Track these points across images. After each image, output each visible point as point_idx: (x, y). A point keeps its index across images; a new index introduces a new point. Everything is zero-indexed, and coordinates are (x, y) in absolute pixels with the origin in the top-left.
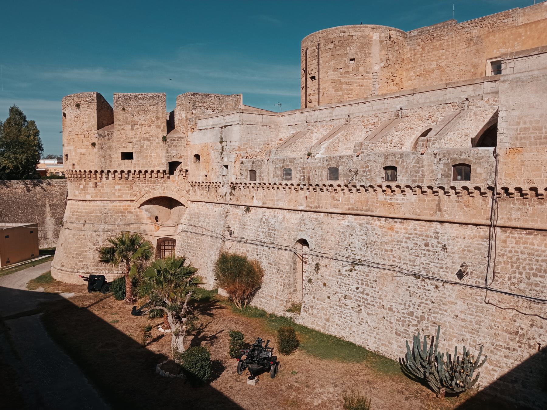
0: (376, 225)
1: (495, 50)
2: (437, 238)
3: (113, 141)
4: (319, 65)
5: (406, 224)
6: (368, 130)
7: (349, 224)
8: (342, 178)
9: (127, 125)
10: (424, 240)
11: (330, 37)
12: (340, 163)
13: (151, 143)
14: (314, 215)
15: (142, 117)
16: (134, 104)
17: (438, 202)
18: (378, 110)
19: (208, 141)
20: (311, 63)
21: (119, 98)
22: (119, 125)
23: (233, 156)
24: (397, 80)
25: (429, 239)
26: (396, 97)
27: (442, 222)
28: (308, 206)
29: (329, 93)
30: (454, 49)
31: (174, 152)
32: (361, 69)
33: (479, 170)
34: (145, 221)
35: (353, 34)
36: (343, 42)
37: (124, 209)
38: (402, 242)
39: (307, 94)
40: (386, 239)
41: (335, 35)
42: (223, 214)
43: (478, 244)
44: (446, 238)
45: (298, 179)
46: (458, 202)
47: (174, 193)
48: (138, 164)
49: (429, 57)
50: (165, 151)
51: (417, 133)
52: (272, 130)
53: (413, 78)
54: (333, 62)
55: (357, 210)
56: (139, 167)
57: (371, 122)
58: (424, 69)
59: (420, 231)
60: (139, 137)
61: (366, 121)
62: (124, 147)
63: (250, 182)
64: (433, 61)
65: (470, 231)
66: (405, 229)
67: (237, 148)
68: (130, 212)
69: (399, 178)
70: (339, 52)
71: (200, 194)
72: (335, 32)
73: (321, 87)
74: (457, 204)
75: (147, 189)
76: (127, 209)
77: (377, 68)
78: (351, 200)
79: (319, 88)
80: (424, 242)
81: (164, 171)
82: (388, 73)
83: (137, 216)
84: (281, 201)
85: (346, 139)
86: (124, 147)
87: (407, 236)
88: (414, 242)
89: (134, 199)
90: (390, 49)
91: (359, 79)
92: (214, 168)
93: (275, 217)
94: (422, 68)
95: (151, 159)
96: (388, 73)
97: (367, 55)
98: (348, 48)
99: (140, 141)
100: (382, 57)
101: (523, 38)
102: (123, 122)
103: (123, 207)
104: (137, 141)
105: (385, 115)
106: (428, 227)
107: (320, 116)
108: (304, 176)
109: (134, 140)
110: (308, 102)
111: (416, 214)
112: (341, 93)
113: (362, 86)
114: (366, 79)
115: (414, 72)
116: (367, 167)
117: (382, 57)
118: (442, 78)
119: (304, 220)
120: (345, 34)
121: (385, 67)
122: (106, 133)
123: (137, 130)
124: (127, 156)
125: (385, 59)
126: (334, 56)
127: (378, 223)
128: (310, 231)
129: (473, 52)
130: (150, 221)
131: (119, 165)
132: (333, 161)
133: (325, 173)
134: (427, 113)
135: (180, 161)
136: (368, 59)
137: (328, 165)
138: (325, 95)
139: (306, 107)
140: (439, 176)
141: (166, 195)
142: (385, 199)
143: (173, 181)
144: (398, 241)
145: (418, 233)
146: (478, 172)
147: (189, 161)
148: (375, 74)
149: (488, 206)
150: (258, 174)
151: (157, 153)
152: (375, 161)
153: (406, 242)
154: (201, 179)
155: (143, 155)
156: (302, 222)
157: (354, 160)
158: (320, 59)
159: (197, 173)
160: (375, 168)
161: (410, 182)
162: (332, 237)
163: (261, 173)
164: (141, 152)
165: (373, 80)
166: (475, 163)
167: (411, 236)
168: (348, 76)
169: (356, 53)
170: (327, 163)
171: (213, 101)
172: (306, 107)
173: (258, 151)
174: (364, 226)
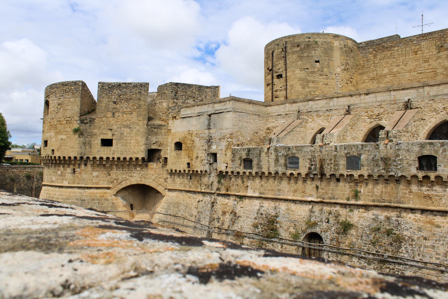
4: (286, 65)
6: (372, 120)
11: (296, 41)
12: (362, 152)
13: (132, 131)
15: (125, 105)
16: (117, 93)
18: (384, 101)
19: (192, 129)
20: (278, 63)
21: (103, 87)
23: (224, 144)
24: (354, 82)
28: (320, 197)
31: (154, 139)
32: (325, 70)
34: (120, 209)
35: (317, 40)
36: (308, 46)
37: (100, 196)
39: (274, 90)
41: (301, 40)
47: (151, 181)
48: (117, 151)
50: (144, 139)
51: (430, 124)
52: (260, 119)
53: (366, 81)
54: (300, 63)
55: (384, 202)
56: (118, 153)
57: (376, 113)
58: (376, 74)
62: (104, 134)
63: (244, 170)
64: (385, 67)
67: (229, 136)
68: (106, 199)
69: (439, 168)
70: (305, 55)
71: (179, 183)
72: (301, 38)
73: (288, 84)
75: (124, 176)
76: (103, 196)
77: (338, 70)
79: (286, 85)
81: (143, 159)
82: (346, 75)
83: (113, 203)
85: (352, 128)
86: (104, 134)
89: (110, 186)
91: (323, 78)
92: (199, 156)
94: (375, 73)
96: (346, 75)
98: (313, 52)
99: (121, 128)
100: (342, 61)
103: (100, 193)
104: (118, 128)
105: (392, 106)
107: (314, 106)
109: (115, 127)
110: (274, 97)
112: (308, 90)
114: (330, 79)
115: (368, 76)
117: (342, 61)
120: (310, 40)
121: (345, 70)
122: (88, 120)
124: (107, 143)
125: (344, 63)
126: (301, 58)
130: (125, 209)
131: (98, 151)
132: (353, 149)
135: (160, 148)
138: (292, 91)
139: (272, 101)
141: (143, 183)
143: (151, 168)
147: (169, 148)
148: (337, 75)
150: (255, 163)
152: (408, 150)
154: (182, 167)
158: (287, 60)
159: (178, 162)
160: (408, 158)
168: (314, 75)
169: (321, 56)
170: (346, 152)
171: (194, 91)
172: (272, 101)
173: (248, 139)
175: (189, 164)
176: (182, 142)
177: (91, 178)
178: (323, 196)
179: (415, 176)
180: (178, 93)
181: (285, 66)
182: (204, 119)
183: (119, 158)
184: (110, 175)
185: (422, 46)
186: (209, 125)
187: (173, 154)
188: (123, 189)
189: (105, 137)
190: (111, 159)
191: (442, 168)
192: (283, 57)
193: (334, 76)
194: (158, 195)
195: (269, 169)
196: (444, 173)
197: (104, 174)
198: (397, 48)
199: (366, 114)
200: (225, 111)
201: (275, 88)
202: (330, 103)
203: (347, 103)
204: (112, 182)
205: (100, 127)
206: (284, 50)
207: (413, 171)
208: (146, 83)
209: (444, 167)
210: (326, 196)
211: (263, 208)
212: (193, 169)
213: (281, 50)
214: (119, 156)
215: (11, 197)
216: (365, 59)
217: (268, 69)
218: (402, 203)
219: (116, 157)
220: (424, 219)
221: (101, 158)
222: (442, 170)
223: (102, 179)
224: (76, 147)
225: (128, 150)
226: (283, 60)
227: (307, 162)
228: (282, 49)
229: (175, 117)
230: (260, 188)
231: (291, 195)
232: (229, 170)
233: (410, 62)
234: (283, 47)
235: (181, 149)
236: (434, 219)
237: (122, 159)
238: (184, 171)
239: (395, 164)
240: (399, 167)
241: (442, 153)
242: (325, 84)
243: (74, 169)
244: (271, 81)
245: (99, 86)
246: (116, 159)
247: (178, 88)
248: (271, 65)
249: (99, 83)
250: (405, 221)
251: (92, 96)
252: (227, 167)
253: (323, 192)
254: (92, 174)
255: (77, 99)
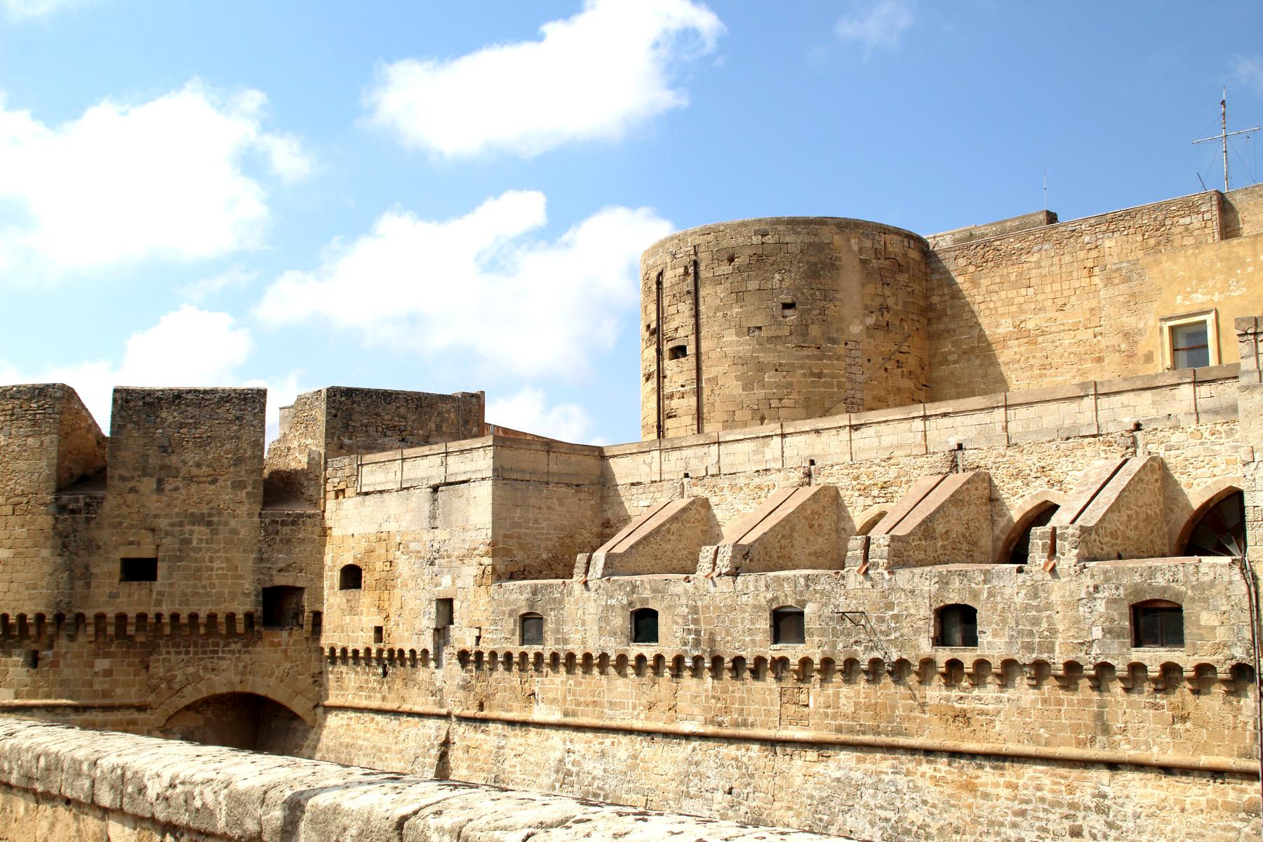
0: (923, 775)
1: (1179, 298)
2: (1101, 810)
3: (100, 526)
5: (1011, 772)
6: (869, 501)
7: (839, 774)
8: (816, 639)
9: (145, 479)
10: (1067, 817)
11: (724, 244)
13: (215, 532)
14: (732, 750)
16: (170, 419)
17: (1099, 707)
18: (899, 447)
20: (673, 310)
21: (127, 401)
22: (122, 478)
25: (1080, 815)
26: (945, 415)
27: (1113, 766)
28: (712, 722)
29: (727, 391)
30: (1057, 287)
31: (282, 558)
32: (815, 331)
33: (1207, 619)
38: (1001, 824)
40: (952, 817)
42: (433, 746)
43: (1225, 829)
44: (1129, 809)
45: (678, 641)
46: (1155, 706)
48: (170, 594)
49: (992, 305)
52: (582, 496)
53: (951, 358)
54: (736, 310)
55: (864, 733)
56: (173, 602)
59: (1053, 791)
60: (178, 515)
61: (864, 477)
62: (131, 543)
65: (1198, 792)
66: (1010, 785)
69: (982, 639)
72: (740, 233)
74: (1152, 712)
75: (191, 670)
77: (856, 329)
78: (843, 701)
80: (1067, 824)
81: (249, 616)
84: (622, 705)
86: (131, 543)
87: (1017, 806)
88: (1038, 824)
89: (150, 699)
90: (889, 280)
91: (808, 356)
93: (603, 754)
95: (210, 578)
97: (828, 296)
98: (777, 276)
99: (181, 524)
101: (1250, 269)
102: (135, 469)
104: (173, 525)
106: (1076, 779)
108: (697, 632)
109: (163, 523)
111: (1039, 744)
113: (820, 375)
114: (830, 358)
116: (890, 606)
118: (1032, 361)
119: (697, 764)
121: (877, 327)
122: (81, 504)
123: (175, 495)
124: (139, 570)
127: (925, 767)
128: (719, 796)
129: (1121, 298)
131: (113, 596)
133: (765, 624)
134: (1035, 458)
136: (831, 305)
137: (773, 600)
140: (1097, 633)
141: (248, 689)
142: (948, 699)
143: (272, 644)
144: (991, 823)
145: (1049, 796)
146: (1203, 623)
149: (1241, 718)
150: (549, 626)
151: (228, 560)
152: (912, 592)
153: (1014, 825)
154: (362, 640)
155: (187, 568)
156: (693, 769)
157: (849, 587)
160: (912, 611)
161: (1015, 650)
162: (791, 813)
163: (560, 622)
164: (180, 559)
165: (848, 361)
166: (1192, 599)
167: (1029, 807)
170: (769, 596)
171: (403, 411)
174: (886, 778)
175: (379, 630)
176: (362, 566)
177: (89, 677)
178: (720, 719)
179: (928, 663)
180: (354, 417)
181: (693, 321)
182: (421, 497)
183: (175, 617)
184: (147, 668)
185: (1107, 250)
186: (433, 517)
187: (338, 600)
188: (188, 708)
189: (134, 553)
190: (151, 619)
191: (990, 639)
192: (689, 292)
193: (840, 349)
194: (295, 724)
195: (583, 643)
196: (992, 652)
197: (129, 665)
198: (1034, 258)
199: (854, 483)
200: (474, 477)
201: (669, 388)
202: (766, 450)
203: (807, 453)
204: (154, 689)
205: (120, 524)
206: (691, 270)
207: (925, 647)
208: (259, 391)
209: (994, 635)
210: (727, 719)
211: (573, 757)
212: (389, 646)
213: (682, 270)
214: (176, 608)
215: (50, 729)
216: (946, 291)
217: (648, 326)
218: (906, 735)
219: (166, 610)
220: (955, 777)
221: (121, 618)
222: (989, 643)
223: (121, 678)
224: (44, 583)
225: (201, 591)
226: (689, 301)
227: (677, 623)
228: (686, 268)
229: (343, 491)
230: (565, 700)
231: (642, 716)
232: (486, 648)
233: (1073, 299)
234: (686, 260)
235: (358, 585)
236: (978, 777)
237: (184, 619)
238: (368, 650)
239: (884, 627)
240: (892, 637)
241: (988, 598)
242: (812, 374)
243: (36, 652)
244: (654, 368)
245: (115, 400)
246: (166, 620)
247: (353, 403)
248: (654, 316)
249: (116, 391)
250: (911, 785)
251: (96, 426)
252: (478, 638)
253: (720, 709)
254: (92, 666)
255: (47, 440)
